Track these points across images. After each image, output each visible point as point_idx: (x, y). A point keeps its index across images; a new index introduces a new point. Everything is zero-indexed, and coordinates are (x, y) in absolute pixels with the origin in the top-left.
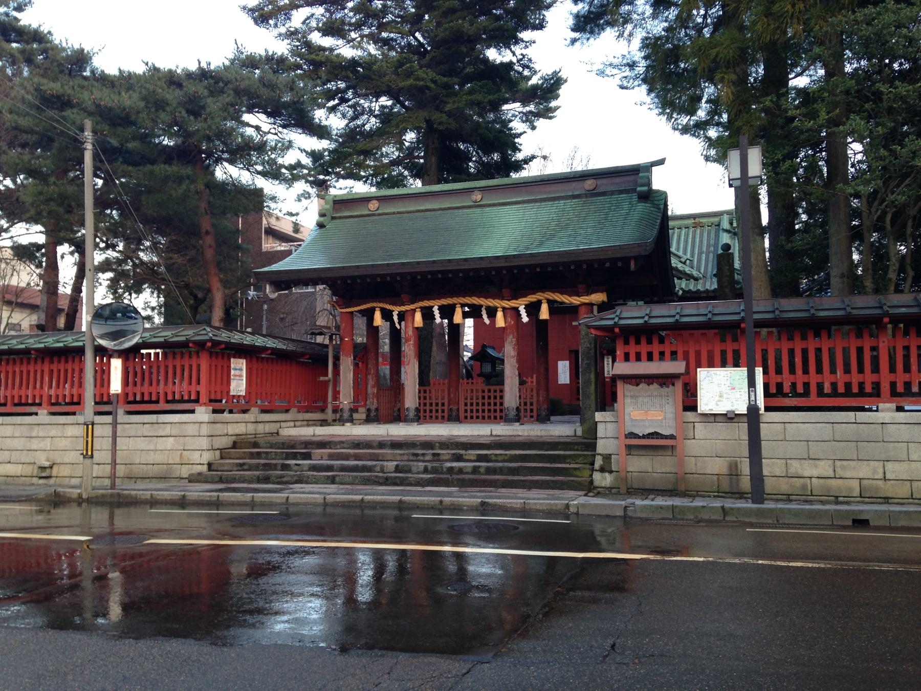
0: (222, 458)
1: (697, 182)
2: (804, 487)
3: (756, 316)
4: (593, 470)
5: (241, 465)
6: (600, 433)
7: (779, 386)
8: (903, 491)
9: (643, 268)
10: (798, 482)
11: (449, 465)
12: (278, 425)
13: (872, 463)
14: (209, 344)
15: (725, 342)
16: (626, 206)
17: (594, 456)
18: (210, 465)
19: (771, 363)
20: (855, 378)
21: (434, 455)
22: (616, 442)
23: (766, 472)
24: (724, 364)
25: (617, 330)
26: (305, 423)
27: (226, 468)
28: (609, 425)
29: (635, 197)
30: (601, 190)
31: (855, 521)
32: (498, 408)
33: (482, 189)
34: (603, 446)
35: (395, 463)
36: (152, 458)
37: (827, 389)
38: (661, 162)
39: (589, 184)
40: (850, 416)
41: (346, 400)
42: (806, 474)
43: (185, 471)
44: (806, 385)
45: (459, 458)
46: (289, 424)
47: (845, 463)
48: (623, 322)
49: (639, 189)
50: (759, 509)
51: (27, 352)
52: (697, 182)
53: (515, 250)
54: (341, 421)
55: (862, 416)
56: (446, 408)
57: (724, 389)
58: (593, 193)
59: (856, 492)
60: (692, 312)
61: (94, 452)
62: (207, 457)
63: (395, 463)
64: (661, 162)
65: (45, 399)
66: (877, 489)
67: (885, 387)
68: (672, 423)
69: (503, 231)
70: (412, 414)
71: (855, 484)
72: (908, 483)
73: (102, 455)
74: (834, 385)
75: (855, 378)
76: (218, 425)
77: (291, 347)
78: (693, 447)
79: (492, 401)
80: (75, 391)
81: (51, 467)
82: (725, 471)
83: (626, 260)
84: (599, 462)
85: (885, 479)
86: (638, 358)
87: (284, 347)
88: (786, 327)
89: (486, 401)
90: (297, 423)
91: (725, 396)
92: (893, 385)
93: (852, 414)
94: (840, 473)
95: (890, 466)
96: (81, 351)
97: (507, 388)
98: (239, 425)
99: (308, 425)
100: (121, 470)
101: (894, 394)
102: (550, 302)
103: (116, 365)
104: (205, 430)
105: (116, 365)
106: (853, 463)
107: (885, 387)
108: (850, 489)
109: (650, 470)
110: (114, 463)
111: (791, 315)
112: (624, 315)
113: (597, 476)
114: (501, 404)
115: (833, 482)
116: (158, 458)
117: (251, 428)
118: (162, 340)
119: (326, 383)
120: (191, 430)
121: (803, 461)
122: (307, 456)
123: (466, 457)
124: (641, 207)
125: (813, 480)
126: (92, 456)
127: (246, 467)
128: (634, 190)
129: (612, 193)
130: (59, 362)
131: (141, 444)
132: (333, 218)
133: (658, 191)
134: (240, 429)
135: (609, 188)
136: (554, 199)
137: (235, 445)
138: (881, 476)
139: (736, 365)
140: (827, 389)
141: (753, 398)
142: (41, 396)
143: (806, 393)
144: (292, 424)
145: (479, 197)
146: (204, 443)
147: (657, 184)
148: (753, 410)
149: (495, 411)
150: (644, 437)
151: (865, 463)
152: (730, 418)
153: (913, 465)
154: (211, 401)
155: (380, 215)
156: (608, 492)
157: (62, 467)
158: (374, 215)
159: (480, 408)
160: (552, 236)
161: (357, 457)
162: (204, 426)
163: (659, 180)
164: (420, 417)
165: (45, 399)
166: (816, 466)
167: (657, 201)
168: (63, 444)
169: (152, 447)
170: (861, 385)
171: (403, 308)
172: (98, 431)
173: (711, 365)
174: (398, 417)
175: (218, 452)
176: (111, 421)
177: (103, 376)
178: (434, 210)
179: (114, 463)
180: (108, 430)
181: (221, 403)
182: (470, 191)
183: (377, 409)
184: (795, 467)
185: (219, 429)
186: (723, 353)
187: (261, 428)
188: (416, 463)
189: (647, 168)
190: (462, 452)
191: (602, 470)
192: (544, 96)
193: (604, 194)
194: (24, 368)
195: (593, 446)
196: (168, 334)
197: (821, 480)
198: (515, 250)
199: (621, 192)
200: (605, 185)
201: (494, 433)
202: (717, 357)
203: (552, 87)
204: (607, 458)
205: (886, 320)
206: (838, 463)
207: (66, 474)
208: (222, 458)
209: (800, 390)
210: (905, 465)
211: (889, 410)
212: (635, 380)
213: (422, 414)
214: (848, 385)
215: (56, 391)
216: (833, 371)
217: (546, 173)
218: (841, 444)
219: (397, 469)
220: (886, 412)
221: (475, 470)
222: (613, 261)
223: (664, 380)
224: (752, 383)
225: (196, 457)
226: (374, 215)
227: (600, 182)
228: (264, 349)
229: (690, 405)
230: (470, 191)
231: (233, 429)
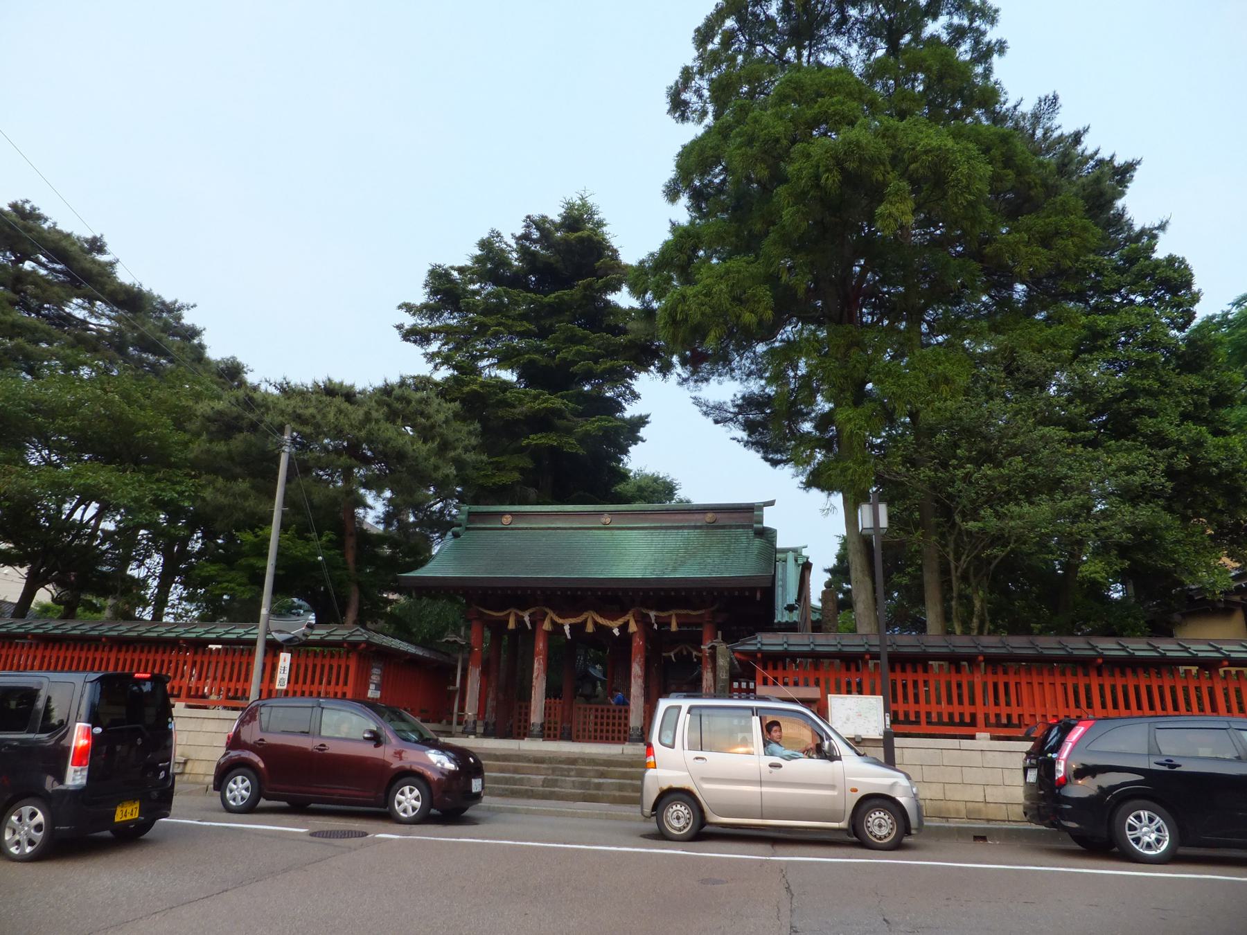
1: (811, 525)
15: (850, 671)
16: (744, 539)
24: (849, 692)
25: (759, 655)
29: (751, 533)
30: (720, 523)
31: (984, 838)
32: (622, 728)
33: (611, 513)
37: (934, 718)
38: (771, 503)
39: (709, 517)
40: (954, 743)
41: (470, 712)
44: (917, 714)
45: (602, 775)
48: (765, 648)
51: (97, 639)
52: (811, 525)
54: (465, 733)
55: (966, 743)
56: (558, 726)
58: (712, 526)
59: (963, 814)
60: (799, 641)
64: (771, 503)
65: (184, 692)
66: (979, 811)
67: (980, 718)
70: (537, 729)
74: (940, 715)
79: (605, 721)
80: (239, 686)
81: (185, 763)
83: (753, 590)
88: (899, 661)
89: (605, 721)
92: (987, 717)
95: (989, 790)
96: (253, 643)
97: (632, 707)
103: (285, 659)
105: (285, 659)
108: (958, 811)
111: (906, 650)
112: (765, 641)
114: (626, 725)
118: (234, 636)
119: (454, 692)
124: (758, 542)
128: (751, 527)
129: (731, 527)
130: (127, 651)
132: (467, 529)
135: (727, 523)
139: (873, 693)
140: (934, 718)
142: (180, 688)
143: (917, 722)
145: (608, 520)
149: (619, 732)
157: (196, 764)
159: (616, 728)
160: (683, 563)
164: (547, 733)
165: (184, 692)
167: (767, 535)
168: (202, 739)
171: (573, 621)
174: (521, 731)
177: (270, 670)
182: (601, 513)
183: (494, 724)
186: (849, 684)
193: (723, 527)
194: (83, 655)
196: (324, 632)
199: (738, 527)
200: (723, 519)
202: (844, 687)
205: (981, 658)
207: (200, 771)
209: (912, 718)
213: (546, 732)
214: (951, 716)
216: (939, 703)
219: (546, 783)
222: (742, 590)
227: (719, 516)
230: (601, 513)
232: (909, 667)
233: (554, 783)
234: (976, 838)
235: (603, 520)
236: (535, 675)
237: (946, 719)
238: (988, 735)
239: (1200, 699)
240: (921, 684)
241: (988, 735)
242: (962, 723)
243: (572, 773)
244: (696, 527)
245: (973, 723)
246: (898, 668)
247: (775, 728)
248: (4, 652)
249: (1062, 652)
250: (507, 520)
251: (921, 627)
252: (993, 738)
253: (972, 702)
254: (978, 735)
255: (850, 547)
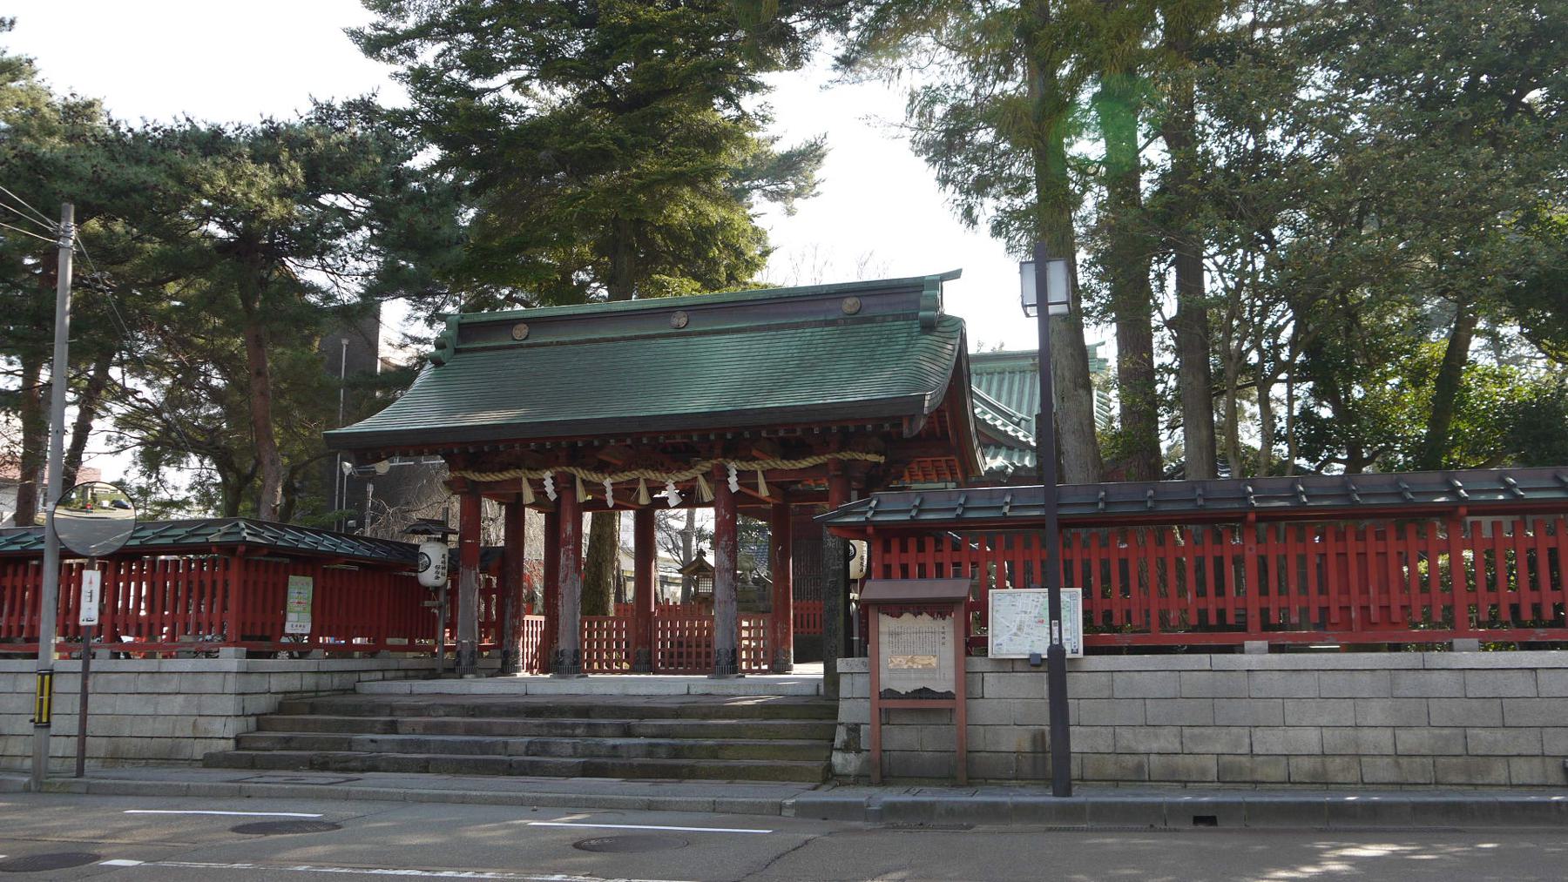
0: (259, 729)
2: (1140, 767)
3: (1064, 511)
4: (832, 748)
5: (288, 740)
6: (844, 691)
7: (1108, 615)
8: (1275, 772)
9: (934, 432)
10: (1130, 761)
11: (611, 742)
12: (356, 676)
13: (1234, 730)
14: (242, 549)
17: (835, 726)
18: (238, 740)
19: (1095, 580)
20: (1212, 605)
21: (589, 725)
22: (867, 704)
23: (1076, 746)
26: (402, 674)
27: (264, 745)
28: (857, 677)
30: (867, 313)
31: (1211, 821)
34: (848, 712)
35: (527, 739)
36: (147, 728)
38: (956, 275)
39: (850, 304)
42: (1142, 749)
43: (198, 750)
45: (627, 732)
46: (373, 676)
47: (1196, 730)
49: (921, 314)
50: (1063, 804)
53: (728, 404)
55: (1221, 660)
57: (1020, 620)
58: (857, 319)
59: (1213, 775)
61: (54, 719)
62: (233, 728)
63: (527, 739)
64: (956, 275)
68: (950, 674)
69: (715, 378)
71: (1211, 763)
72: (1284, 759)
73: (66, 721)
75: (1212, 605)
76: (253, 677)
77: (380, 554)
78: (983, 711)
82: (1027, 746)
84: (841, 736)
85: (1252, 754)
86: (905, 574)
87: (368, 553)
90: (388, 675)
91: (1026, 629)
92: (1264, 612)
93: (1206, 657)
94: (1190, 746)
98: (284, 675)
99: (407, 678)
100: (96, 746)
101: (1267, 627)
102: (646, 480)
104: (232, 684)
106: (1209, 731)
107: (1254, 618)
108: (1203, 771)
109: (918, 747)
110: (83, 735)
113: (838, 758)
115: (1178, 759)
116: (161, 728)
117: (309, 682)
118: (170, 541)
120: (212, 684)
121: (1137, 730)
122: (392, 727)
123: (641, 730)
125: (1152, 757)
126: (48, 724)
127: (293, 744)
131: (133, 705)
132: (457, 351)
133: (951, 318)
134: (293, 683)
136: (797, 326)
137: (281, 709)
138: (1246, 750)
141: (1056, 635)
144: (379, 675)
145: (683, 321)
146: (230, 705)
147: (950, 308)
148: (1056, 651)
150: (908, 696)
151: (1225, 730)
152: (1033, 663)
153: (1291, 732)
154: (244, 638)
155: (529, 346)
156: (861, 779)
157: (11, 741)
158: (521, 346)
161: (469, 730)
162: (230, 678)
163: (953, 302)
166: (1156, 736)
169: (150, 711)
170: (1221, 614)
171: (744, 466)
172: (60, 684)
173: (1002, 586)
175: (253, 719)
176: (80, 669)
178: (613, 340)
179: (83, 735)
180: (74, 684)
181: (261, 638)
184: (1128, 739)
185: (256, 683)
186: (922, 566)
187: (325, 681)
188: (558, 740)
189: (936, 282)
190: (634, 722)
191: (846, 748)
192: (791, 170)
193: (871, 320)
195: (833, 712)
197: (1162, 758)
198: (728, 404)
199: (897, 318)
201: (693, 691)
203: (812, 154)
204: (854, 729)
206: (1186, 731)
208: (259, 729)
210: (1279, 732)
211: (1259, 651)
212: (896, 608)
215: (8, 621)
216: (1182, 592)
217: (801, 284)
218: (1192, 702)
220: (1255, 656)
221: (651, 751)
223: (937, 608)
224: (1055, 612)
225: (217, 727)
226: (521, 346)
228: (333, 557)
229: (975, 644)
231: (276, 684)
232: (912, 544)
233: (544, 749)
234: (1198, 820)
235: (675, 321)
236: (561, 575)
237: (1213, 621)
238: (1264, 644)
239: (1304, 578)
240: (1372, 557)
241: (1264, 644)
242: (1223, 626)
243: (578, 731)
244: (828, 323)
245: (1242, 627)
246: (895, 545)
247: (498, 664)
248: (7, 582)
249: (1396, 500)
250: (520, 332)
251: (740, 474)
252: (1274, 649)
253: (1323, 589)
254: (1248, 644)
255: (1054, 339)
